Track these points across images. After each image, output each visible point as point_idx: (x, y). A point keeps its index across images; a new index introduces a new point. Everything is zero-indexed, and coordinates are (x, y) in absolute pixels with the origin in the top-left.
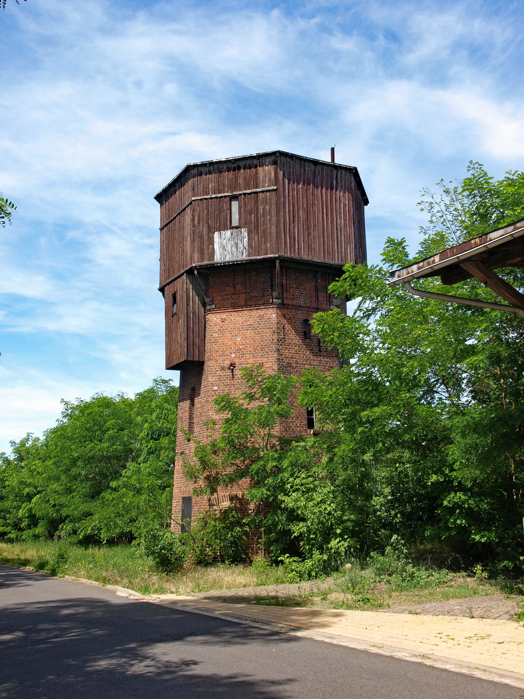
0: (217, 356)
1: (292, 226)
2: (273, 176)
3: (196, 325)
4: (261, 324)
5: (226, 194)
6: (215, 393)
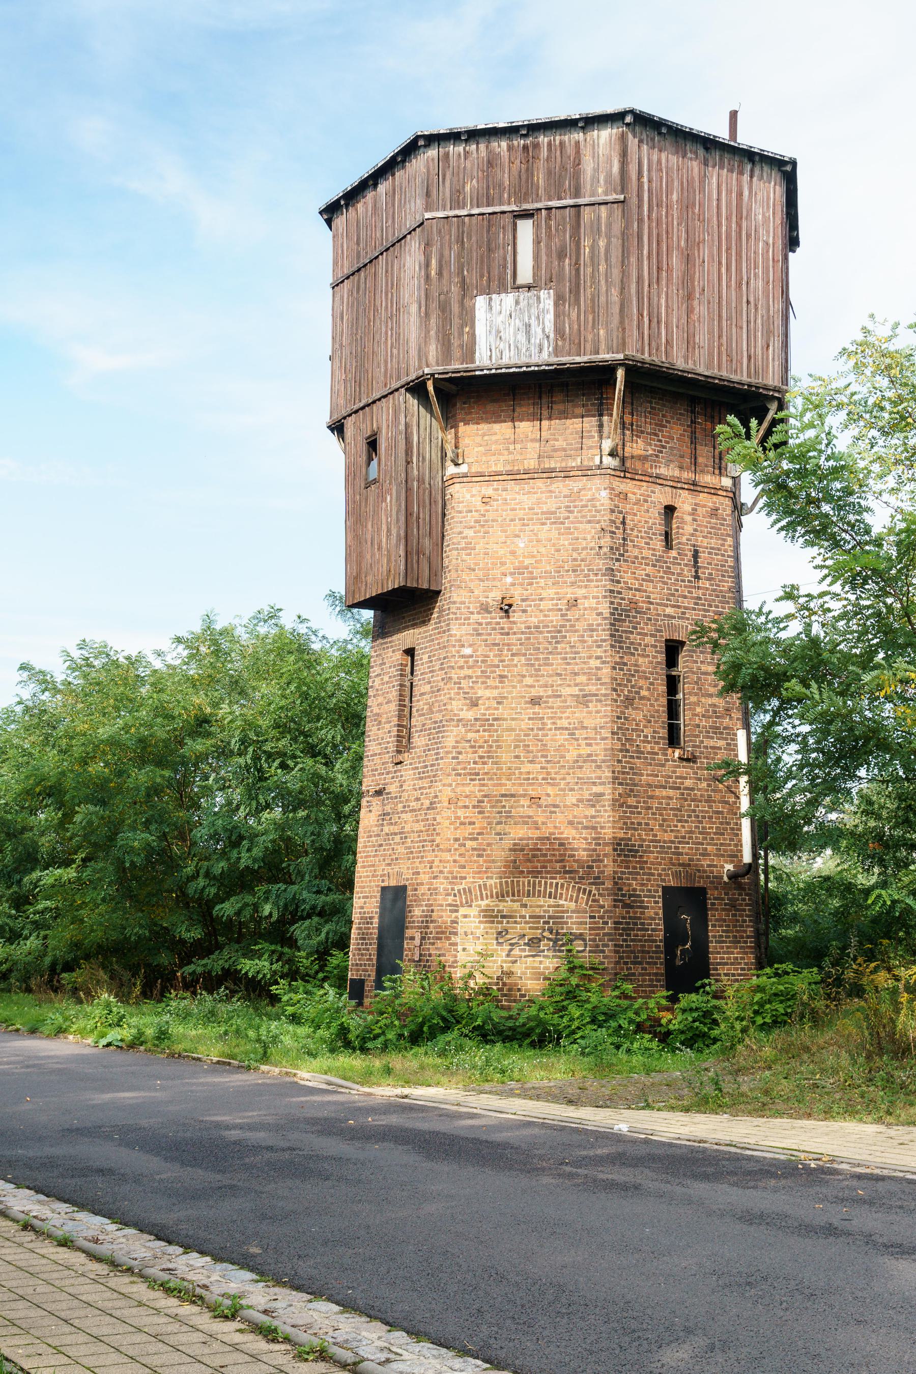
0: (471, 580)
1: (654, 291)
3: (424, 507)
5: (505, 208)
6: (467, 662)
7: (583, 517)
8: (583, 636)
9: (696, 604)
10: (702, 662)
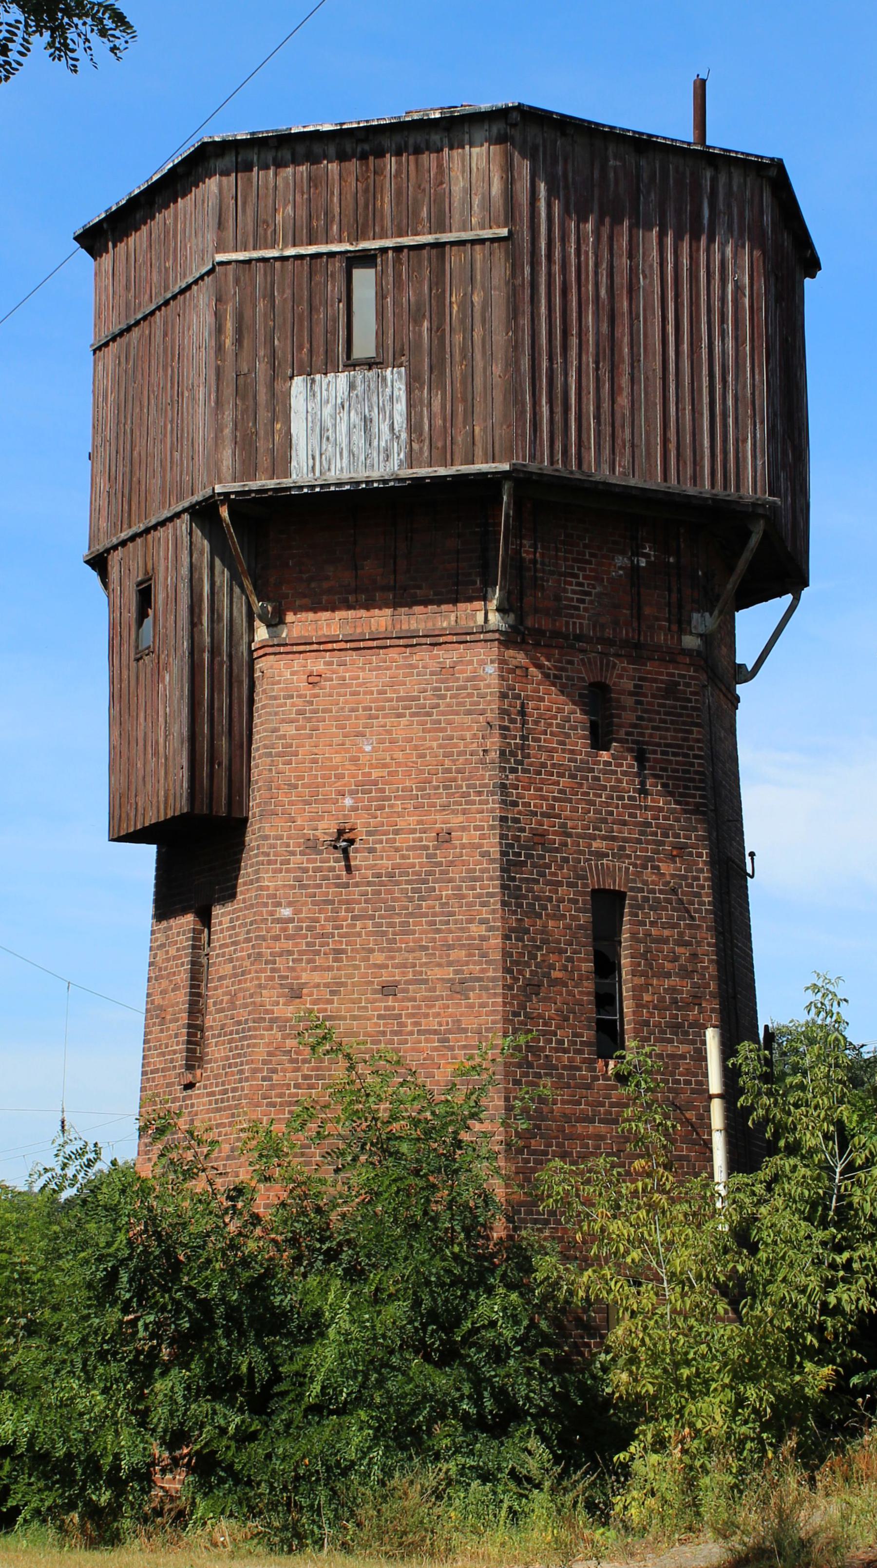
0: (291, 803)
2: (496, 188)
3: (221, 691)
4: (443, 697)
6: (285, 929)
7: (458, 704)
8: (460, 888)
9: (642, 833)
10: (653, 924)
